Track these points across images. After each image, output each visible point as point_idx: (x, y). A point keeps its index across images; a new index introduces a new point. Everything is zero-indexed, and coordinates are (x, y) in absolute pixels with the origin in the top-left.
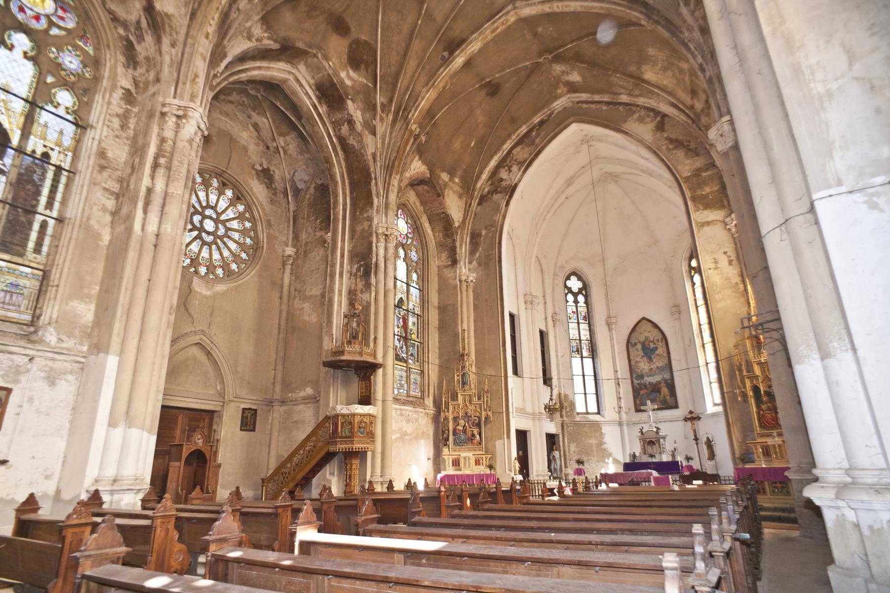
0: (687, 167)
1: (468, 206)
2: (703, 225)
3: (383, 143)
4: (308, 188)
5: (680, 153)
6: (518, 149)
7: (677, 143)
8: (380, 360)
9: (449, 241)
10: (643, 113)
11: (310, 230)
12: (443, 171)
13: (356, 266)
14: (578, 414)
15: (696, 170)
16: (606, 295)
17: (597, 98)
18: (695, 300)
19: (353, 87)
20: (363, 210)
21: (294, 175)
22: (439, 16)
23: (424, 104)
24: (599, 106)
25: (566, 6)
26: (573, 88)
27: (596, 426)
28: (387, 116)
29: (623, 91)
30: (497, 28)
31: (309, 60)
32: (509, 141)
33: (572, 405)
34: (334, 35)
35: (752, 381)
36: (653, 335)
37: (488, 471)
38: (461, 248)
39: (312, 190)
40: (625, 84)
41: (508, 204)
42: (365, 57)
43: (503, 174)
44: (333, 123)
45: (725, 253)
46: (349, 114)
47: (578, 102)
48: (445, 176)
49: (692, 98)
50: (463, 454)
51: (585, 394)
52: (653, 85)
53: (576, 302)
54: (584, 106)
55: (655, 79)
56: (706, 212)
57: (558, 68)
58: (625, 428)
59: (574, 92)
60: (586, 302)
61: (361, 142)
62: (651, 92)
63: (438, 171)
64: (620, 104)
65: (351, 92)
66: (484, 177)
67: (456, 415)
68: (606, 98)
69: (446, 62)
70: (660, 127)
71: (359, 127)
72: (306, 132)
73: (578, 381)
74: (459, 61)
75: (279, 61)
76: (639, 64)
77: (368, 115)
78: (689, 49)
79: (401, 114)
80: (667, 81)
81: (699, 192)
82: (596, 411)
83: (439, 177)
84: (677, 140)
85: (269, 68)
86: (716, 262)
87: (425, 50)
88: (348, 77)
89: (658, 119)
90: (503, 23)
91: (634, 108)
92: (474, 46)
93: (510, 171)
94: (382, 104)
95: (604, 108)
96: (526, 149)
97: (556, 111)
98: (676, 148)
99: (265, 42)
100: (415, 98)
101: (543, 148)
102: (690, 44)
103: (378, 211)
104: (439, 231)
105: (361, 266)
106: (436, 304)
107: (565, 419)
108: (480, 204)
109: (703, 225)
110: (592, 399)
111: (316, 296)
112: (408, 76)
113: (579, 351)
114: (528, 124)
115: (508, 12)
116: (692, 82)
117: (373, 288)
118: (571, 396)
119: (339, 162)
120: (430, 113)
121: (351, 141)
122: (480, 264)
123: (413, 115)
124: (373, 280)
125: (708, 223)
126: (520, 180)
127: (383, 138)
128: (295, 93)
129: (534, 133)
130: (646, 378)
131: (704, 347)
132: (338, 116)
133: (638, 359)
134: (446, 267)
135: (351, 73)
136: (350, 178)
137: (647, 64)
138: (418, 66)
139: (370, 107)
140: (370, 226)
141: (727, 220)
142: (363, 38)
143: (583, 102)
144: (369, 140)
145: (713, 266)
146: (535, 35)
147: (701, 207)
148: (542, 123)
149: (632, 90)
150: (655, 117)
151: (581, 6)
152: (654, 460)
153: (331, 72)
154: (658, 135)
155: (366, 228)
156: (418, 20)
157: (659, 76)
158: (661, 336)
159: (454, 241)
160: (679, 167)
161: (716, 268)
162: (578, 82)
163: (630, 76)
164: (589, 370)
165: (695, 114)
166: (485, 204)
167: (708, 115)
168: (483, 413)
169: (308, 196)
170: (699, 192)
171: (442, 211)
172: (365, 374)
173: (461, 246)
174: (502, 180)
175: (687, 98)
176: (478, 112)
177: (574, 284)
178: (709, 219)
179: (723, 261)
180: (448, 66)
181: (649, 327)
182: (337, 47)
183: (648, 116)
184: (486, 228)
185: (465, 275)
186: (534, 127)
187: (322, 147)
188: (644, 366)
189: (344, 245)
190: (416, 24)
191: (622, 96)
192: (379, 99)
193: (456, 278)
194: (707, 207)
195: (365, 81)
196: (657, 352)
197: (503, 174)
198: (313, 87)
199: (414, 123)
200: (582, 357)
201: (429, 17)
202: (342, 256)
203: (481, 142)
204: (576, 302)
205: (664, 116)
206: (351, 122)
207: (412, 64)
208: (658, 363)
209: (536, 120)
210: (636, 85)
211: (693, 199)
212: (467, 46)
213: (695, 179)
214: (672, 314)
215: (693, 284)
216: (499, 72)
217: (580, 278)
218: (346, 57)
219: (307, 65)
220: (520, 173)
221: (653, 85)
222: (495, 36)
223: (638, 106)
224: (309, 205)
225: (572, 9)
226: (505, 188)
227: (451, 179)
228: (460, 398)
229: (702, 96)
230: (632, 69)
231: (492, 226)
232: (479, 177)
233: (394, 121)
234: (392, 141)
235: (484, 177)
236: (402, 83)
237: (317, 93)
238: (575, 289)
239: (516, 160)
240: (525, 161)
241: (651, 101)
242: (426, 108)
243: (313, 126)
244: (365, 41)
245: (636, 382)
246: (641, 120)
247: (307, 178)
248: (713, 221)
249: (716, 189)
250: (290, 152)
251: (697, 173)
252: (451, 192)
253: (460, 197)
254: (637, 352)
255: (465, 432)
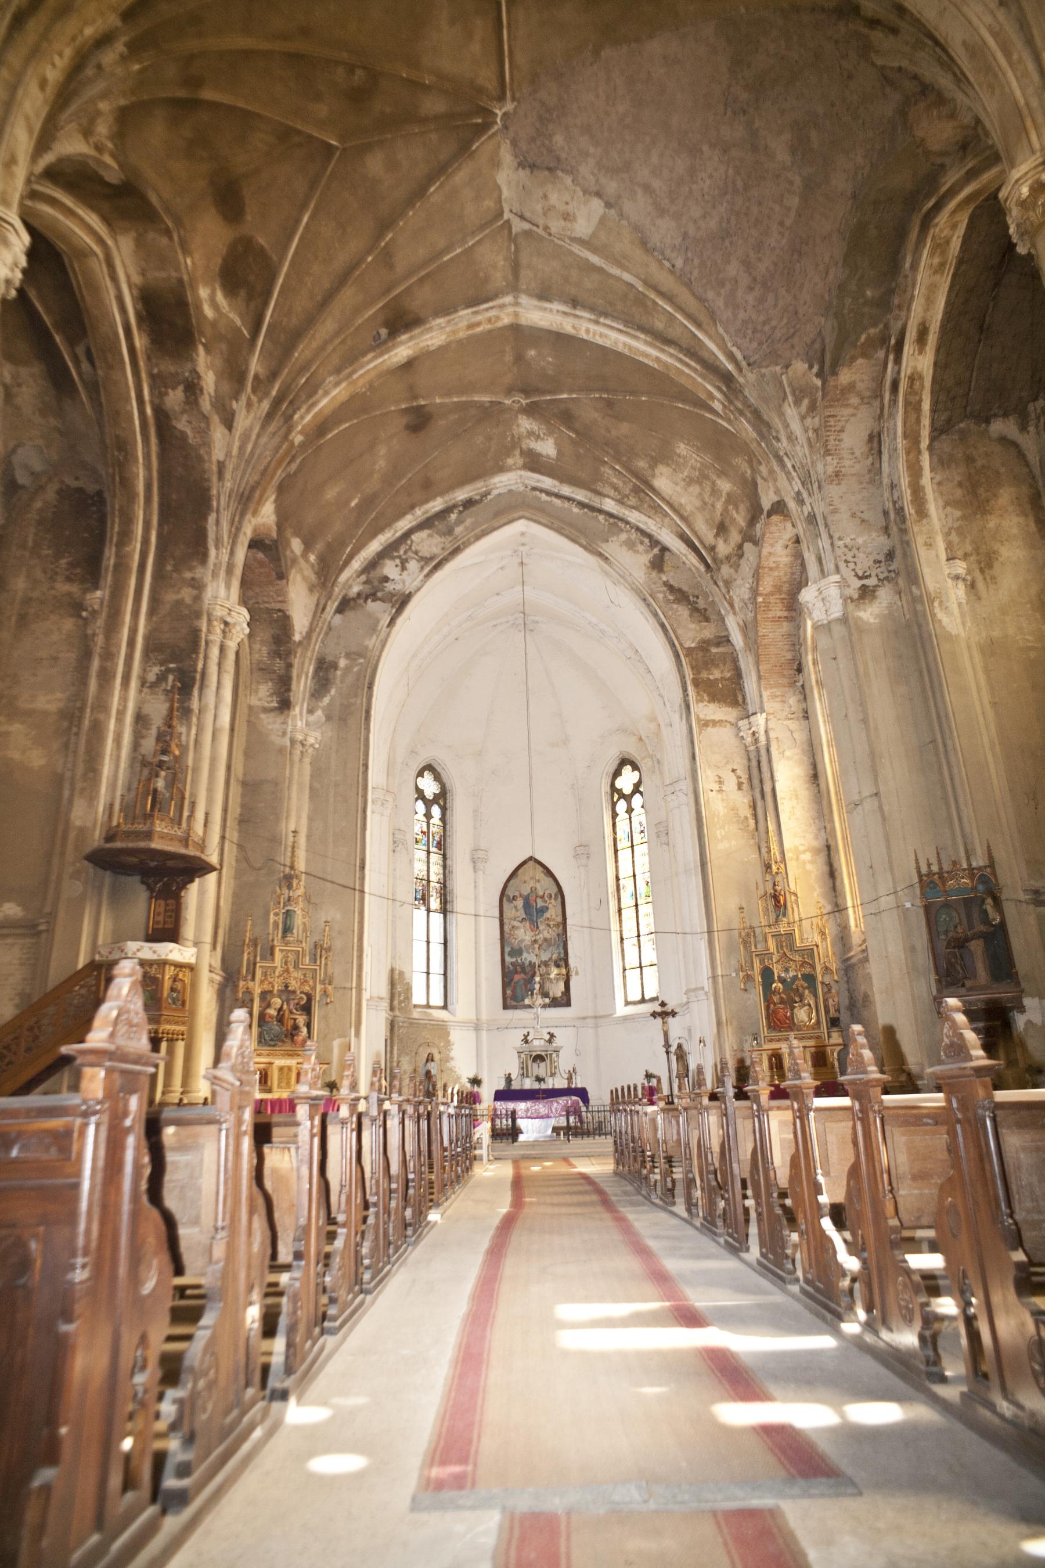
0: (691, 634)
1: (320, 609)
2: (706, 724)
3: (242, 448)
4: (42, 488)
5: (683, 611)
6: (424, 534)
7: (680, 595)
8: (214, 859)
9: (279, 664)
10: (634, 535)
11: (39, 574)
12: (297, 534)
13: (156, 670)
14: (415, 1006)
15: (704, 641)
16: (476, 811)
17: (566, 490)
18: (615, 840)
19: (214, 324)
20: (182, 563)
21: (14, 451)
22: (402, 261)
23: (324, 403)
24: (566, 505)
25: (601, 335)
26: (534, 463)
27: (442, 1030)
28: (260, 401)
29: (612, 493)
30: (479, 324)
31: (151, 235)
32: (409, 517)
33: (408, 990)
34: (213, 210)
35: (762, 961)
36: (545, 886)
37: (325, 1093)
38: (299, 682)
39: (50, 495)
40: (621, 484)
41: (392, 623)
42: (252, 278)
43: (390, 568)
44: (152, 377)
45: (733, 771)
46: (194, 372)
47: (534, 489)
48: (296, 545)
49: (717, 535)
50: (279, 1062)
51: (428, 973)
52: (663, 499)
53: (428, 816)
54: (544, 497)
55: (670, 492)
56: (712, 706)
57: (525, 424)
58: (484, 1033)
59: (533, 470)
60: (443, 819)
61: (204, 432)
62: (656, 508)
63: (289, 532)
64: (600, 511)
65: (208, 331)
66: (356, 564)
67: (266, 987)
68: (581, 495)
69: (380, 345)
70: (658, 564)
71: (206, 404)
72: (80, 374)
73: (419, 948)
74: (402, 351)
75: (93, 208)
76: (654, 462)
77: (226, 387)
78: (783, 465)
79: (283, 408)
80: (688, 499)
81: (704, 675)
82: (440, 1003)
83: (288, 544)
84: (680, 590)
85: (70, 213)
86: (721, 782)
87: (357, 310)
88: (211, 302)
89: (656, 551)
90: (489, 320)
91: (621, 525)
92: (434, 335)
93: (404, 568)
94: (256, 377)
95: (576, 510)
96: (437, 539)
97: (495, 492)
98: (678, 601)
99: (108, 159)
100: (312, 389)
101: (467, 544)
102: (785, 459)
103: (215, 575)
104: (262, 642)
105: (169, 671)
106: (241, 776)
107: (397, 1013)
108: (340, 610)
109: (706, 724)
110: (437, 982)
111: (45, 713)
112: (315, 344)
113: (424, 899)
114: (447, 498)
115: (502, 307)
116: (726, 510)
117: (194, 720)
118: (407, 976)
119: (147, 456)
120: (321, 428)
121: (182, 424)
122: (329, 718)
123: (302, 418)
124: (195, 705)
125: (714, 723)
126: (419, 589)
127: (245, 437)
128: (95, 289)
129: (453, 517)
130: (525, 955)
131: (620, 915)
132: (168, 366)
133: (516, 924)
134: (265, 710)
135: (220, 296)
136: (162, 496)
137: (668, 465)
138: (337, 333)
139: (234, 374)
140: (198, 598)
141: (741, 723)
142: (261, 241)
143: (542, 491)
144: (218, 432)
145: (716, 787)
146: (519, 358)
147: (706, 697)
148: (469, 503)
149: (627, 496)
150: (652, 547)
151: (625, 344)
152: (543, 1086)
153: (185, 277)
154: (654, 574)
155: (188, 600)
156: (369, 253)
157: (678, 489)
158: (556, 889)
159: (290, 666)
160: (680, 632)
161: (720, 791)
162: (548, 457)
163: (636, 474)
164: (437, 936)
165: (714, 560)
166: (350, 614)
167: (736, 567)
168: (319, 987)
169: (38, 504)
170: (704, 675)
171: (278, 606)
172: (167, 886)
173: (299, 677)
174: (386, 579)
175: (708, 535)
176: (382, 450)
177: (429, 786)
178: (717, 717)
179: (731, 783)
180: (382, 354)
181: (539, 873)
182: (207, 239)
183: (642, 543)
184: (348, 655)
185: (302, 731)
186: (455, 506)
187: (119, 416)
188: (523, 935)
189: (136, 624)
190: (362, 260)
191: (607, 500)
192: (255, 365)
193: (284, 734)
194: (714, 698)
195: (239, 323)
196: (547, 915)
197: (390, 568)
198: (135, 292)
199: (301, 432)
200: (428, 910)
201: (387, 258)
202: (131, 643)
203: (369, 502)
204: (428, 816)
205: (664, 549)
206: (193, 388)
207: (327, 326)
208: (546, 933)
209: (461, 495)
210: (636, 490)
211: (696, 683)
212: (422, 333)
213: (701, 654)
214: (576, 856)
215: (615, 815)
216: (441, 396)
217: (437, 777)
218: (220, 261)
219: (140, 243)
220: (421, 577)
221: (663, 499)
222: (471, 337)
223: (627, 523)
224: (40, 523)
225: (608, 344)
226: (393, 595)
227: (305, 555)
228: (278, 956)
229: (735, 537)
230: (642, 464)
231: (360, 655)
232: (347, 562)
233: (269, 416)
234: (258, 452)
235: (356, 564)
236: (301, 352)
237: (140, 306)
238: (429, 795)
239: (416, 553)
240: (432, 558)
241: (650, 522)
242: (326, 412)
243: (110, 367)
244: (262, 249)
245: (508, 959)
246: (630, 545)
247: (38, 466)
248: (721, 721)
249: (728, 675)
250: (18, 401)
251: (704, 646)
252: (299, 578)
253: (311, 589)
254: (515, 911)
255: (280, 1019)
